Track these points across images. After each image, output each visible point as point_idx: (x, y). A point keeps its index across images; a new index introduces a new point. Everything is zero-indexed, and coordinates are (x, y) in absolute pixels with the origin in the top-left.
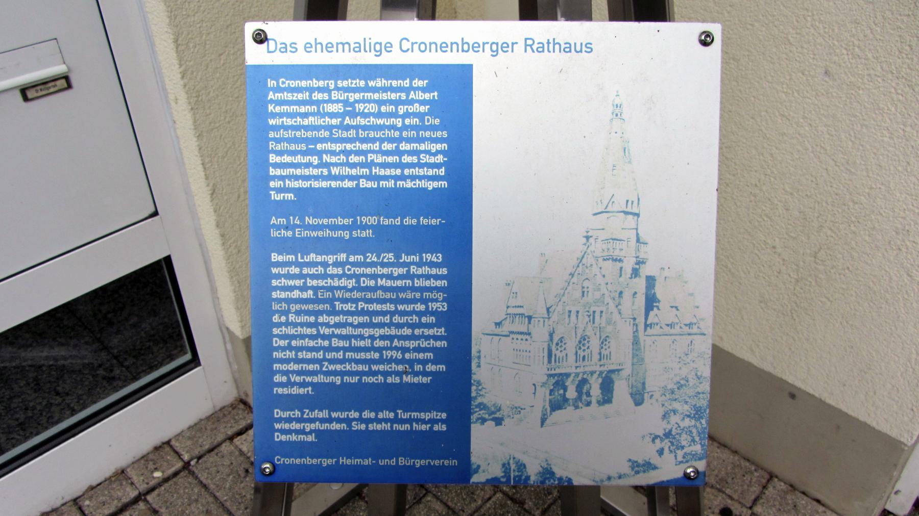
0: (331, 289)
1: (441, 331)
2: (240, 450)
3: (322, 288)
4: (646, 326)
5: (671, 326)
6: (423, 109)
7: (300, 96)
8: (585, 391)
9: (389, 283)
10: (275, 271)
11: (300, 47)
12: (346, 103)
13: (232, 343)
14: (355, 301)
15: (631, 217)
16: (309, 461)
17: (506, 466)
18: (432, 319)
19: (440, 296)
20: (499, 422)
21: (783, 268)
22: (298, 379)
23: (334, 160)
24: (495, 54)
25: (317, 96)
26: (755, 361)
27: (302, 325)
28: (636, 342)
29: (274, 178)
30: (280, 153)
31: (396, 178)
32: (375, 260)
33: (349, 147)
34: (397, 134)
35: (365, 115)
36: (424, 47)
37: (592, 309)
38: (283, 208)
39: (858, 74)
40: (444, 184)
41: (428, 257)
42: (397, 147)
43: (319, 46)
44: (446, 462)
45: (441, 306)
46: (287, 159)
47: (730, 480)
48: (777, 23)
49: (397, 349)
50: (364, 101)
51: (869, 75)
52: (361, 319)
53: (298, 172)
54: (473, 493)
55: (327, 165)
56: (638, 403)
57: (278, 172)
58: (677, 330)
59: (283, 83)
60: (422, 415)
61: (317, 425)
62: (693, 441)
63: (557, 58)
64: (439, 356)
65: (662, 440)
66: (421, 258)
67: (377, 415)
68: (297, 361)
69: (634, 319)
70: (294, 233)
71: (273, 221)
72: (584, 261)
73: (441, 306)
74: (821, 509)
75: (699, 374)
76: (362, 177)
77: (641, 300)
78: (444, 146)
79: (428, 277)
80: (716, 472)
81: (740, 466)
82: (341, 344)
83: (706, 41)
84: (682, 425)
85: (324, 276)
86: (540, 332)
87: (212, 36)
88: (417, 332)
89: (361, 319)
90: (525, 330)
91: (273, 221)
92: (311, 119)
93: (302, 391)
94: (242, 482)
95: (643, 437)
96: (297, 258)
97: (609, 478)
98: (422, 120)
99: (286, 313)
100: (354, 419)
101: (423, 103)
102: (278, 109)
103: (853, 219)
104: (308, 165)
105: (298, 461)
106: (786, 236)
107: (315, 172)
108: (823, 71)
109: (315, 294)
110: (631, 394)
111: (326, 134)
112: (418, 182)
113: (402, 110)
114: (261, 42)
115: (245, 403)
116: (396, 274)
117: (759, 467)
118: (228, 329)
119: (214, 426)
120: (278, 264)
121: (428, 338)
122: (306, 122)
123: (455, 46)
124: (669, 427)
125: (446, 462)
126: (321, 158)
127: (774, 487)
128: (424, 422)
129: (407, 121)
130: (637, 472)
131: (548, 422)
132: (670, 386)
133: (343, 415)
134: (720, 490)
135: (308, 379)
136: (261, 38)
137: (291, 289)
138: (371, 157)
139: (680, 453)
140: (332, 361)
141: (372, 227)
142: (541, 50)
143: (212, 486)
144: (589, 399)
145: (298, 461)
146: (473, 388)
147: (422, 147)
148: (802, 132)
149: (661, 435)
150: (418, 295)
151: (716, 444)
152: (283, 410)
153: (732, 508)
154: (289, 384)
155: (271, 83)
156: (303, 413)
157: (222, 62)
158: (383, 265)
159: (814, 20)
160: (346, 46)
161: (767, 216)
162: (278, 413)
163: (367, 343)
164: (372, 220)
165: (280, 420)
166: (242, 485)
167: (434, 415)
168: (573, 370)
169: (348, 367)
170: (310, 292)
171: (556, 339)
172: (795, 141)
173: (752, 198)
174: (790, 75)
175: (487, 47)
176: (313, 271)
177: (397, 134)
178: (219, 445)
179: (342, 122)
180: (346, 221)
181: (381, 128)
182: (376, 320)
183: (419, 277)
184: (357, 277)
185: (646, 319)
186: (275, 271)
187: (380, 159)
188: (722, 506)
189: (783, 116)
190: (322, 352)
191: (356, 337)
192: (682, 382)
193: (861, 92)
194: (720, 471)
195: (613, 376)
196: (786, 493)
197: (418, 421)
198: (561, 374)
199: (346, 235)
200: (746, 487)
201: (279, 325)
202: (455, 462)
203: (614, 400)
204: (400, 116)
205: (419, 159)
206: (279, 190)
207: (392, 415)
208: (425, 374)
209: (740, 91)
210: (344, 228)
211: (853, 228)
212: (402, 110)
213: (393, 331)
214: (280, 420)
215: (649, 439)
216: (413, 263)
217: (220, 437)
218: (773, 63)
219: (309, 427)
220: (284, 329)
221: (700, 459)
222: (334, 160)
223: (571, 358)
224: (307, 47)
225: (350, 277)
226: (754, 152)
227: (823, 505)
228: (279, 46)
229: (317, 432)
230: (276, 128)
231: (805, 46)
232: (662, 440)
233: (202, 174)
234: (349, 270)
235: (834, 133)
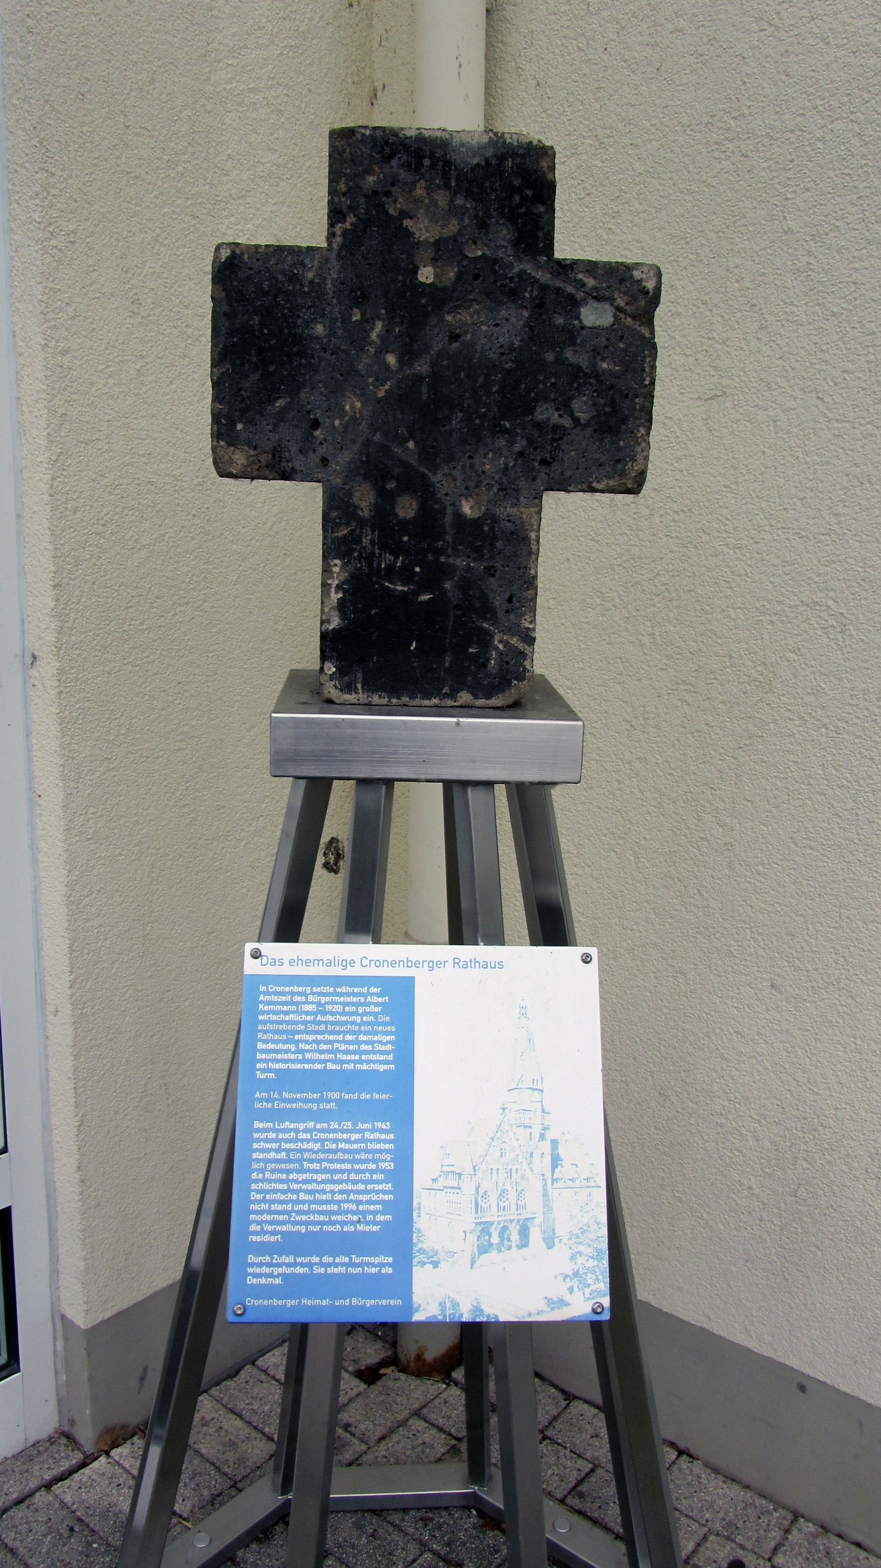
0: (300, 1151)
1: (389, 1186)
2: (62, 1502)
3: (293, 1150)
4: (553, 1180)
5: (572, 1180)
6: (377, 1009)
7: (284, 998)
8: (506, 1237)
9: (347, 1146)
10: (256, 1135)
11: (286, 962)
12: (319, 1004)
13: (66, 1339)
14: (320, 1161)
15: (536, 1092)
16: (276, 1302)
17: (442, 1304)
18: (381, 1176)
19: (388, 1157)
20: (436, 1265)
21: (764, 1214)
22: (270, 1228)
23: (308, 1047)
24: (431, 969)
25: (297, 998)
26: (753, 1345)
27: (276, 1181)
28: (545, 1194)
29: (260, 1061)
30: (266, 1042)
31: (355, 1062)
32: (337, 1127)
33: (319, 1037)
34: (357, 1028)
35: (333, 1014)
36: (379, 964)
37: (510, 1167)
38: (265, 1085)
39: (803, 986)
40: (392, 1067)
41: (379, 1125)
42: (357, 1038)
43: (300, 962)
44: (392, 1302)
45: (389, 1166)
46: (271, 1046)
47: (740, 1524)
48: (718, 935)
49: (352, 1201)
50: (332, 1003)
51: (813, 987)
52: (324, 1176)
53: (279, 1056)
54: (390, 1554)
55: (302, 1051)
56: (550, 1247)
57: (264, 1056)
58: (577, 1184)
59: (272, 988)
60: (372, 1260)
61: (283, 1270)
62: (598, 1279)
63: (477, 972)
64: (387, 1207)
65: (571, 1279)
66: (374, 1126)
67: (334, 1259)
68: (270, 1212)
69: (543, 1175)
70: (273, 1105)
71: (257, 1095)
72: (501, 1128)
73: (389, 1166)
74: (862, 1554)
75: (598, 1220)
76: (329, 1061)
77: (548, 1159)
78: (393, 1038)
79: (378, 1141)
80: (721, 1515)
81: (752, 1504)
82: (307, 1197)
83: (586, 959)
84: (587, 1265)
85: (296, 1140)
86: (468, 1187)
87: (108, 942)
88: (369, 1187)
89: (324, 1176)
90: (456, 1185)
91: (257, 1095)
92: (291, 1016)
93: (273, 1239)
94: (64, 1545)
95: (556, 1277)
96: (274, 1126)
97: (530, 1315)
98: (376, 1018)
99: (263, 1171)
100: (315, 1264)
101: (377, 1004)
102: (266, 1008)
103: (826, 1146)
104: (287, 1051)
105: (266, 1302)
106: (761, 1173)
107: (293, 1056)
108: (767, 984)
109: (288, 1155)
110: (544, 1239)
111: (302, 1027)
112: (372, 1065)
113: (361, 1010)
114: (256, 958)
115: (68, 1436)
116: (353, 1139)
117: (779, 1505)
118: (63, 1317)
119: (25, 1467)
120: (259, 1130)
121: (378, 1192)
122: (287, 1018)
123: (401, 963)
124: (576, 1267)
125: (392, 1302)
126: (297, 1046)
127: (800, 1530)
128: (373, 1265)
129: (365, 1019)
130: (553, 1309)
131: (477, 1264)
132: (576, 1231)
133: (306, 1260)
134: (727, 1538)
135: (279, 1228)
136: (256, 955)
137: (268, 1151)
138: (336, 1045)
139: (587, 1291)
140: (299, 1213)
141: (335, 1100)
142: (465, 966)
143: (22, 1551)
144: (509, 1243)
145: (266, 1302)
146: (415, 1235)
147: (376, 1038)
148: (759, 1050)
149: (571, 1274)
150: (370, 1156)
151: (721, 1478)
152: (256, 1256)
153: (744, 1560)
154: (263, 1232)
155: (262, 988)
156: (272, 1259)
157: (114, 971)
158: (344, 1131)
159: (752, 932)
160: (321, 962)
161: (738, 1150)
162: (251, 1259)
163: (328, 1197)
164: (336, 1095)
165: (252, 1265)
166: (66, 1549)
167: (382, 1259)
168: (496, 1219)
169: (312, 1218)
170: (284, 1154)
171: (481, 1192)
172: (754, 1061)
173: (720, 1129)
174: (739, 989)
175: (426, 964)
176: (287, 1136)
177: (357, 1028)
178: (31, 1495)
179: (315, 1019)
180: (315, 1096)
181: (346, 1023)
182: (337, 1177)
183: (371, 1141)
184: (322, 1141)
185: (553, 1175)
186: (256, 1135)
187: (343, 1047)
188: (731, 1558)
189: (737, 1033)
190: (290, 1205)
191: (319, 1192)
192: (585, 1228)
193: (808, 1004)
194: (727, 1513)
195: (529, 1224)
196: (815, 1536)
197: (369, 1264)
198: (486, 1222)
199: (315, 1107)
200: (762, 1532)
201: (257, 1181)
202: (399, 1302)
203: (530, 1245)
204: (359, 1015)
205: (373, 1047)
206: (263, 1071)
207: (347, 1260)
208: (375, 1223)
209: (692, 1007)
210: (313, 1101)
211: (828, 1157)
212: (361, 1010)
213: (350, 1187)
214: (252, 1265)
215: (560, 1278)
216: (367, 1130)
217: (32, 1485)
218: (720, 976)
219: (277, 1271)
220: (260, 1184)
221: (604, 1296)
222: (308, 1047)
223: (494, 1208)
224: (291, 962)
225: (316, 1141)
226: (714, 1074)
227: (865, 1550)
228: (270, 961)
229: (283, 1275)
230: (264, 1022)
231: (748, 958)
232: (571, 1279)
233: (72, 1101)
234: (316, 1135)
235: (790, 1049)
